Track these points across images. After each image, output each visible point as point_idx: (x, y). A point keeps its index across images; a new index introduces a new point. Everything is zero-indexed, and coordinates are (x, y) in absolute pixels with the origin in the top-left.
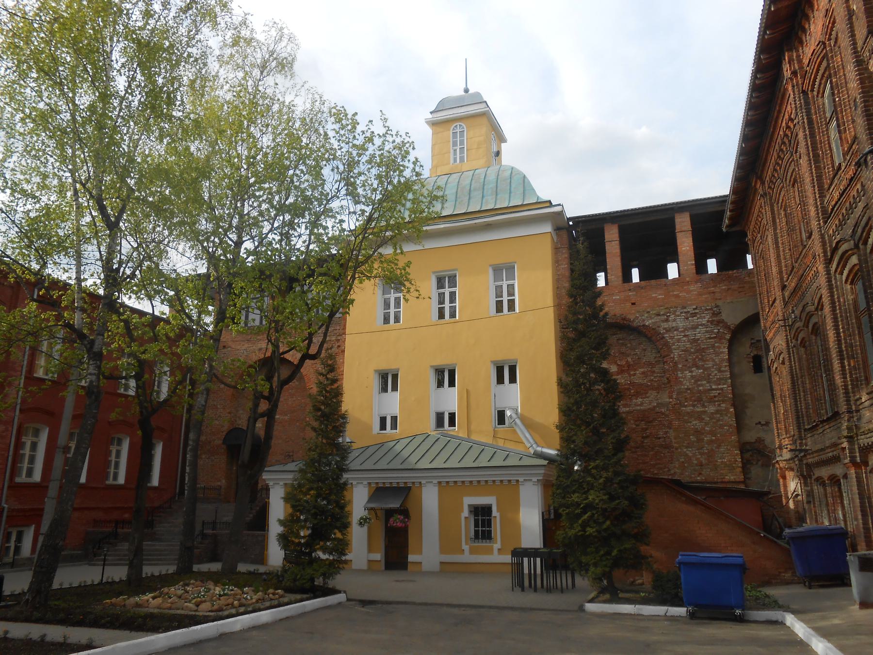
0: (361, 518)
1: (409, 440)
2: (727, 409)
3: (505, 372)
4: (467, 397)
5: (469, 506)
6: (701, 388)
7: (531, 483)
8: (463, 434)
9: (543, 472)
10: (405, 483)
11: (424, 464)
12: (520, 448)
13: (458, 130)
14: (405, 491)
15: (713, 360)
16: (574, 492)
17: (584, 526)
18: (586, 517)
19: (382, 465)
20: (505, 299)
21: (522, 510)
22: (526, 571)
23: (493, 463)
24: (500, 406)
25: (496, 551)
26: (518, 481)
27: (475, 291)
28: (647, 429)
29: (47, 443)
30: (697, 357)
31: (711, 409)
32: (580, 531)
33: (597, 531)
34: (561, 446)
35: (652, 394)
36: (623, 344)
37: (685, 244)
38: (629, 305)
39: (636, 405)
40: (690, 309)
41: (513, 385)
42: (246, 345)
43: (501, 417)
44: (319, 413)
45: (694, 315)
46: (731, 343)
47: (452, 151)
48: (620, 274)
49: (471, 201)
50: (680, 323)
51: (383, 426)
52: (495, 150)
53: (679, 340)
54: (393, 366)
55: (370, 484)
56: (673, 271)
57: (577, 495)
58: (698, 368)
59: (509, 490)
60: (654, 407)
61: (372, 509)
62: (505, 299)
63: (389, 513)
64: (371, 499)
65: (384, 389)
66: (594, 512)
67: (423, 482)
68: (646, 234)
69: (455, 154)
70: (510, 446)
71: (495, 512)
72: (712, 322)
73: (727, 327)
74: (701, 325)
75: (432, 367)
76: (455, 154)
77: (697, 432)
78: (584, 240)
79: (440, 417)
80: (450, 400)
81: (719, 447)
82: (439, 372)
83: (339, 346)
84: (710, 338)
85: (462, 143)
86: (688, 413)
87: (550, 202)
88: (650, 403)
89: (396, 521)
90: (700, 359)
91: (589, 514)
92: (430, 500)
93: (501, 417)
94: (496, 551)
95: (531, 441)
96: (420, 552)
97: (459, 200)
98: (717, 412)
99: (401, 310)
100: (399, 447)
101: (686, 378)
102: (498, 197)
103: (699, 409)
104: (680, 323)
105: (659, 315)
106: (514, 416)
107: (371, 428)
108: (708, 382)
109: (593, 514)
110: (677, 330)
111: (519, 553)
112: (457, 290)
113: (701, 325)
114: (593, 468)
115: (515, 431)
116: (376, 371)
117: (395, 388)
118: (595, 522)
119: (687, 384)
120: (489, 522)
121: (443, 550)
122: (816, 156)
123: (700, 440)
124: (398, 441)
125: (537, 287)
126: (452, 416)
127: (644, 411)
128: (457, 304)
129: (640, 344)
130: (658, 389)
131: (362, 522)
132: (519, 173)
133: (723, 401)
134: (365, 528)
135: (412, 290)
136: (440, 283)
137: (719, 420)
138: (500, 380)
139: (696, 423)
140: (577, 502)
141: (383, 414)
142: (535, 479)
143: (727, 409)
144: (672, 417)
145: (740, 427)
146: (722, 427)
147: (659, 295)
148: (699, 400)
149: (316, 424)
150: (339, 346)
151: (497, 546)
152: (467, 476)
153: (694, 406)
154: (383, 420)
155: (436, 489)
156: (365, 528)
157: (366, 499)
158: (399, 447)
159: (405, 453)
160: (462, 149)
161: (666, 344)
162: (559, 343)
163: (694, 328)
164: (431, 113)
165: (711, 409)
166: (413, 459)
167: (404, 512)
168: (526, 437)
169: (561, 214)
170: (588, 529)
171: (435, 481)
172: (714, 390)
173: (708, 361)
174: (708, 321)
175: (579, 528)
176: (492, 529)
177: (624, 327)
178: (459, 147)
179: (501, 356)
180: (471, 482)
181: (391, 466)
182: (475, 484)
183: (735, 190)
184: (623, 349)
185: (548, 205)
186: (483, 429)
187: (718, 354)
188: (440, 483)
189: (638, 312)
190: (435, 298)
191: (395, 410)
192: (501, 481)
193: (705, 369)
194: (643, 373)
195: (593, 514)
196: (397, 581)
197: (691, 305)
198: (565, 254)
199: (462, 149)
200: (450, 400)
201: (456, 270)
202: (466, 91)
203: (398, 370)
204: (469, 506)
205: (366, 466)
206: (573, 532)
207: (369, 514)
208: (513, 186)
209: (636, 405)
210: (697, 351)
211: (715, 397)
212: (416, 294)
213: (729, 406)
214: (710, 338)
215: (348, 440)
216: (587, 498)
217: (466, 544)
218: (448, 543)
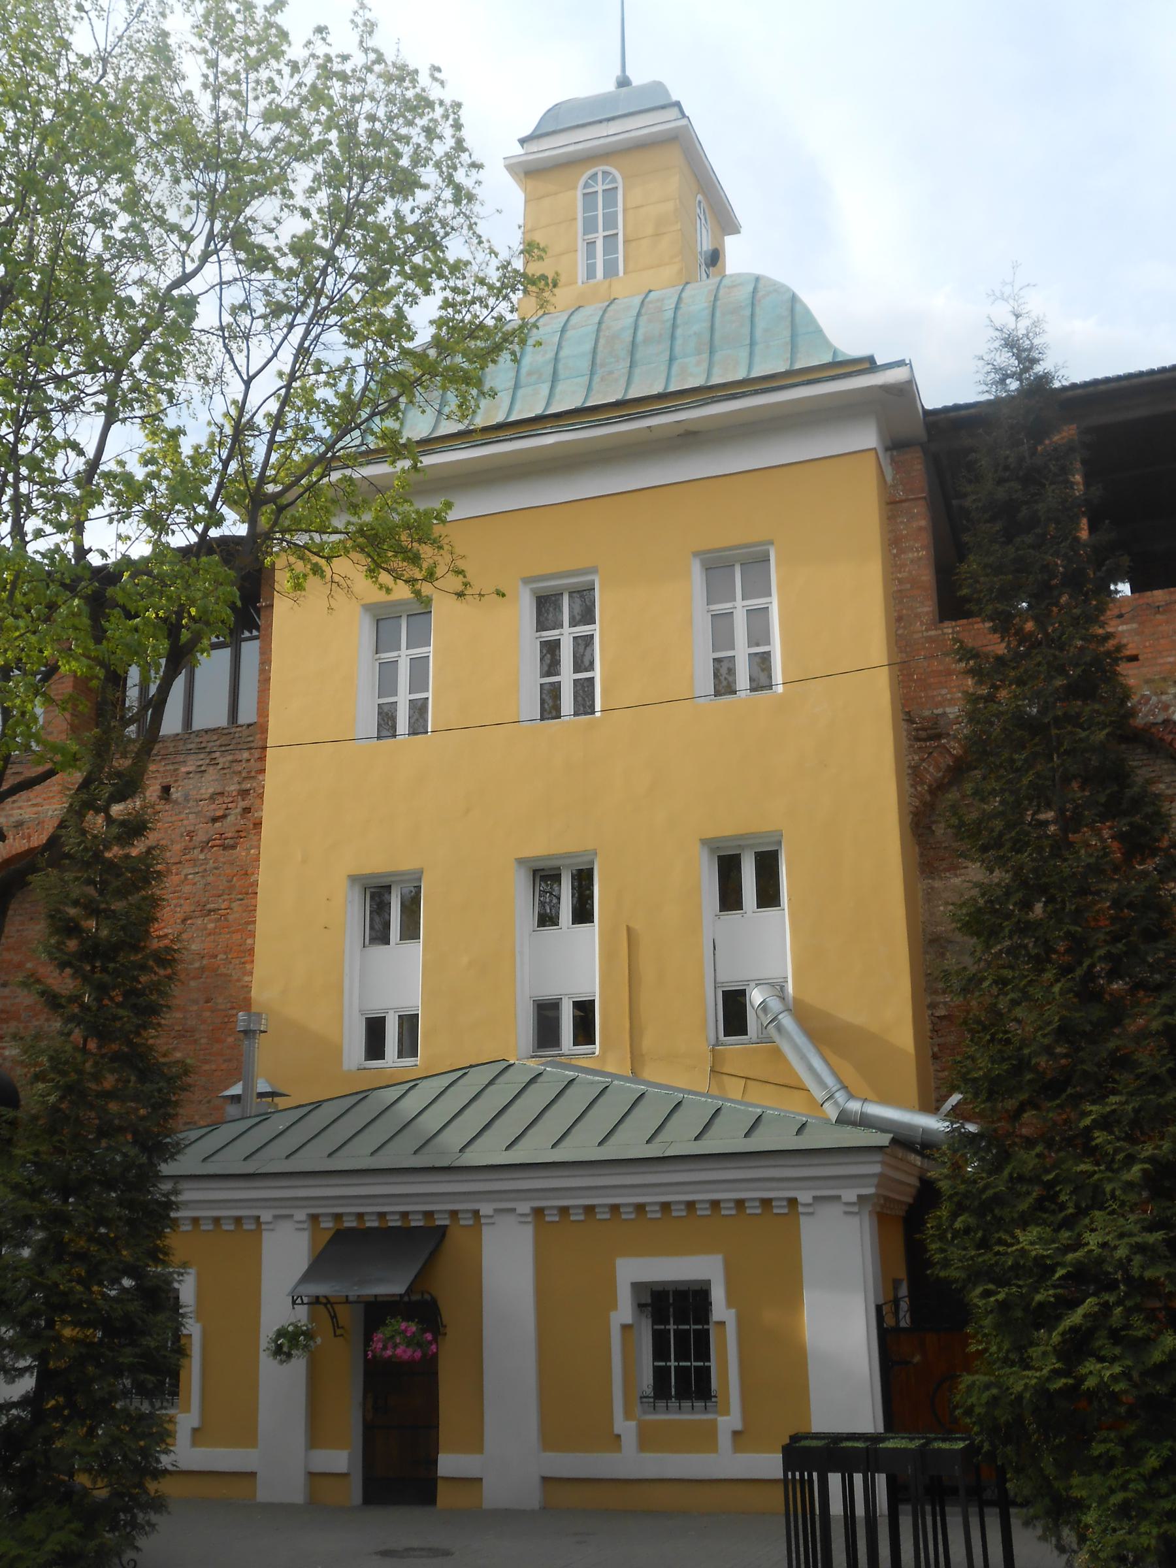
0: (281, 1333)
1: (446, 1080)
3: (745, 874)
4: (628, 950)
5: (637, 1287)
7: (836, 1210)
8: (617, 1064)
9: (877, 1169)
10: (429, 1215)
11: (489, 1152)
12: (795, 1107)
13: (600, 188)
14: (426, 1243)
16: (1024, 1222)
17: (1077, 1347)
18: (1076, 1317)
19: (358, 1156)
21: (811, 1297)
22: (836, 1507)
23: (708, 1146)
24: (731, 978)
25: (724, 1440)
26: (793, 1202)
27: (651, 628)
32: (1056, 1373)
33: (1126, 1375)
41: (770, 913)
43: (734, 1008)
44: (72, 945)
47: (581, 247)
49: (637, 371)
51: (375, 1049)
52: (707, 246)
54: (405, 863)
55: (314, 1218)
57: (1034, 1232)
59: (764, 1229)
61: (316, 1301)
63: (377, 1313)
64: (318, 1267)
65: (380, 935)
66: (1111, 1298)
67: (486, 1209)
69: (591, 254)
70: (764, 1100)
71: (720, 1309)
75: (521, 861)
76: (591, 254)
79: (546, 1016)
80: (577, 962)
82: (544, 877)
83: (247, 810)
85: (610, 221)
87: (871, 360)
89: (398, 1341)
91: (1090, 1304)
92: (507, 1268)
93: (734, 1008)
94: (724, 1440)
95: (830, 1081)
96: (475, 1444)
97: (600, 372)
99: (430, 695)
100: (411, 1105)
102: (718, 357)
106: (775, 1005)
107: (337, 1052)
109: (1106, 1308)
111: (811, 1456)
112: (596, 630)
114: (1096, 1125)
115: (777, 1053)
116: (353, 879)
117: (411, 931)
118: (1115, 1336)
120: (703, 1339)
121: (553, 1436)
124: (414, 1084)
125: (834, 621)
126: (585, 1010)
128: (597, 674)
131: (288, 1343)
132: (778, 289)
134: (298, 1365)
135: (440, 571)
136: (546, 607)
138: (730, 899)
140: (1038, 1260)
141: (375, 1011)
142: (850, 1195)
149: (64, 983)
150: (247, 810)
151: (729, 1421)
152: (627, 1190)
154: (375, 1028)
155: (528, 1232)
156: (298, 1365)
157: (300, 1262)
158: (411, 1105)
159: (431, 1122)
160: (610, 240)
162: (907, 783)
164: (522, 141)
166: (454, 1138)
167: (423, 1310)
168: (811, 1068)
169: (906, 392)
170: (1091, 1365)
171: (524, 1207)
175: (1053, 1363)
176: (713, 1364)
178: (601, 233)
179: (735, 821)
180: (640, 1208)
181: (383, 1161)
182: (654, 1214)
185: (867, 365)
186: (678, 1055)
188: (538, 1212)
189: (1148, 682)
191: (413, 998)
192: (740, 1204)
195: (1106, 1308)
196: (386, 1553)
198: (919, 520)
199: (610, 240)
200: (577, 962)
201: (594, 570)
202: (624, 82)
203: (418, 876)
204: (637, 1287)
205: (308, 1160)
206: (1032, 1377)
207: (312, 1317)
208: (761, 325)
212: (456, 583)
215: (262, 1086)
216: (1078, 1244)
217: (628, 1415)
218: (568, 1412)
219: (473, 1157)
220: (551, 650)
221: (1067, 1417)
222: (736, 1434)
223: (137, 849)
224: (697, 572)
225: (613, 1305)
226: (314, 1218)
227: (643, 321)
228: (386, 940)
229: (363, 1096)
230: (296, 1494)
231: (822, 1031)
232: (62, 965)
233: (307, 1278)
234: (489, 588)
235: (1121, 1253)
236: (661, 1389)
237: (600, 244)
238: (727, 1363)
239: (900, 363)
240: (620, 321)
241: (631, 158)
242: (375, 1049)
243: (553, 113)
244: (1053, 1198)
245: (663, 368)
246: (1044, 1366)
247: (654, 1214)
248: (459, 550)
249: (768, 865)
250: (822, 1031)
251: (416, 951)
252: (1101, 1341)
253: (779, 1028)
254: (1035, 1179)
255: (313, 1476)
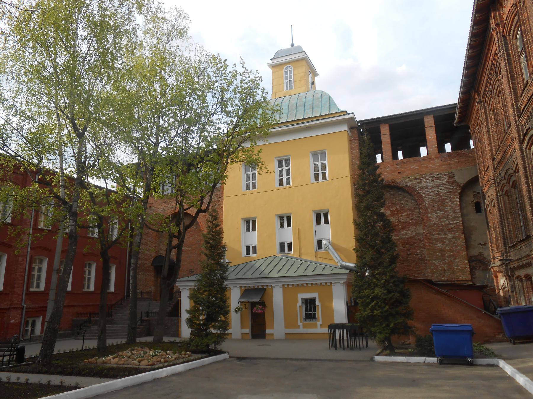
0: (236, 308)
2: (460, 236)
3: (321, 217)
4: (298, 233)
5: (302, 299)
6: (443, 223)
7: (339, 284)
8: (297, 256)
9: (346, 277)
10: (262, 286)
11: (274, 274)
12: (332, 263)
13: (288, 70)
14: (262, 291)
15: (450, 206)
16: (366, 289)
17: (372, 309)
18: (373, 304)
19: (248, 275)
21: (334, 301)
23: (315, 273)
24: (319, 238)
25: (319, 326)
26: (331, 283)
27: (302, 168)
28: (409, 250)
30: (440, 204)
31: (450, 236)
32: (370, 312)
35: (413, 228)
39: (403, 235)
40: (435, 175)
42: (164, 206)
44: (209, 245)
45: (437, 178)
47: (285, 83)
49: (297, 113)
51: (248, 252)
52: (311, 81)
53: (428, 194)
54: (253, 216)
55: (241, 287)
57: (367, 291)
58: (441, 211)
59: (326, 289)
60: (414, 236)
61: (242, 302)
63: (253, 304)
65: (248, 230)
67: (273, 285)
69: (287, 84)
70: (325, 262)
71: (318, 303)
72: (449, 182)
73: (458, 185)
74: (442, 184)
75: (276, 215)
76: (287, 84)
77: (442, 251)
79: (282, 245)
80: (288, 235)
81: (455, 259)
83: (219, 204)
84: (448, 192)
85: (291, 77)
86: (435, 239)
88: (412, 233)
89: (258, 309)
90: (442, 206)
91: (375, 302)
92: (278, 296)
93: (320, 244)
95: (339, 258)
96: (272, 327)
97: (290, 113)
99: (257, 181)
100: (258, 265)
101: (434, 217)
103: (443, 236)
105: (415, 179)
106: (328, 244)
107: (241, 253)
108: (447, 220)
110: (427, 188)
111: (333, 327)
112: (290, 167)
113: (442, 184)
115: (328, 253)
116: (242, 219)
117: (254, 229)
118: (379, 307)
119: (434, 221)
120: (315, 308)
121: (287, 326)
123: (443, 255)
124: (257, 261)
125: (340, 164)
126: (290, 245)
127: (408, 238)
128: (291, 176)
129: (404, 197)
131: (237, 310)
132: (327, 94)
133: (457, 231)
134: (239, 314)
135: (263, 168)
136: (280, 163)
137: (454, 243)
138: (319, 222)
139: (440, 245)
142: (342, 282)
143: (460, 236)
146: (456, 247)
148: (442, 230)
149: (207, 252)
150: (219, 204)
151: (319, 323)
152: (300, 281)
153: (438, 234)
154: (248, 248)
155: (281, 289)
156: (239, 314)
158: (258, 265)
159: (262, 268)
160: (291, 81)
161: (421, 197)
163: (438, 186)
164: (271, 60)
165: (450, 236)
166: (267, 271)
167: (262, 304)
169: (353, 119)
171: (281, 285)
172: (451, 224)
173: (447, 206)
174: (446, 182)
176: (316, 313)
179: (319, 207)
180: (302, 284)
181: (253, 276)
182: (305, 285)
185: (345, 113)
186: (309, 252)
191: (256, 243)
193: (445, 212)
194: (407, 215)
195: (378, 302)
197: (436, 172)
198: (356, 143)
199: (291, 81)
200: (288, 235)
201: (290, 155)
202: (292, 45)
203: (256, 218)
204: (302, 299)
205: (240, 276)
207: (241, 305)
208: (323, 102)
209: (403, 235)
210: (440, 201)
211: (452, 228)
213: (461, 234)
214: (448, 192)
215: (227, 261)
216: (374, 292)
217: (301, 322)
218: (290, 322)
219: (272, 275)
220: (281, 171)
221: (372, 319)
222: (321, 325)
223: (218, 228)
224: (311, 156)
225: (298, 302)
226: (241, 287)
227: (298, 101)
228: (249, 231)
229: (248, 263)
230: (239, 337)
231: (337, 248)
232: (207, 249)
233: (240, 298)
234: (272, 171)
235: (380, 294)
236: (307, 317)
237: (288, 82)
238: (319, 312)
239: (352, 113)
240: (294, 101)
241: (294, 64)
242: (248, 252)
243: (277, 53)
244: (370, 285)
245: (303, 112)
246: (368, 312)
247: (305, 285)
248: (266, 164)
249: (326, 215)
250: (337, 248)
251: (256, 233)
252: (377, 308)
253: (329, 248)
254: (367, 282)
255: (242, 334)
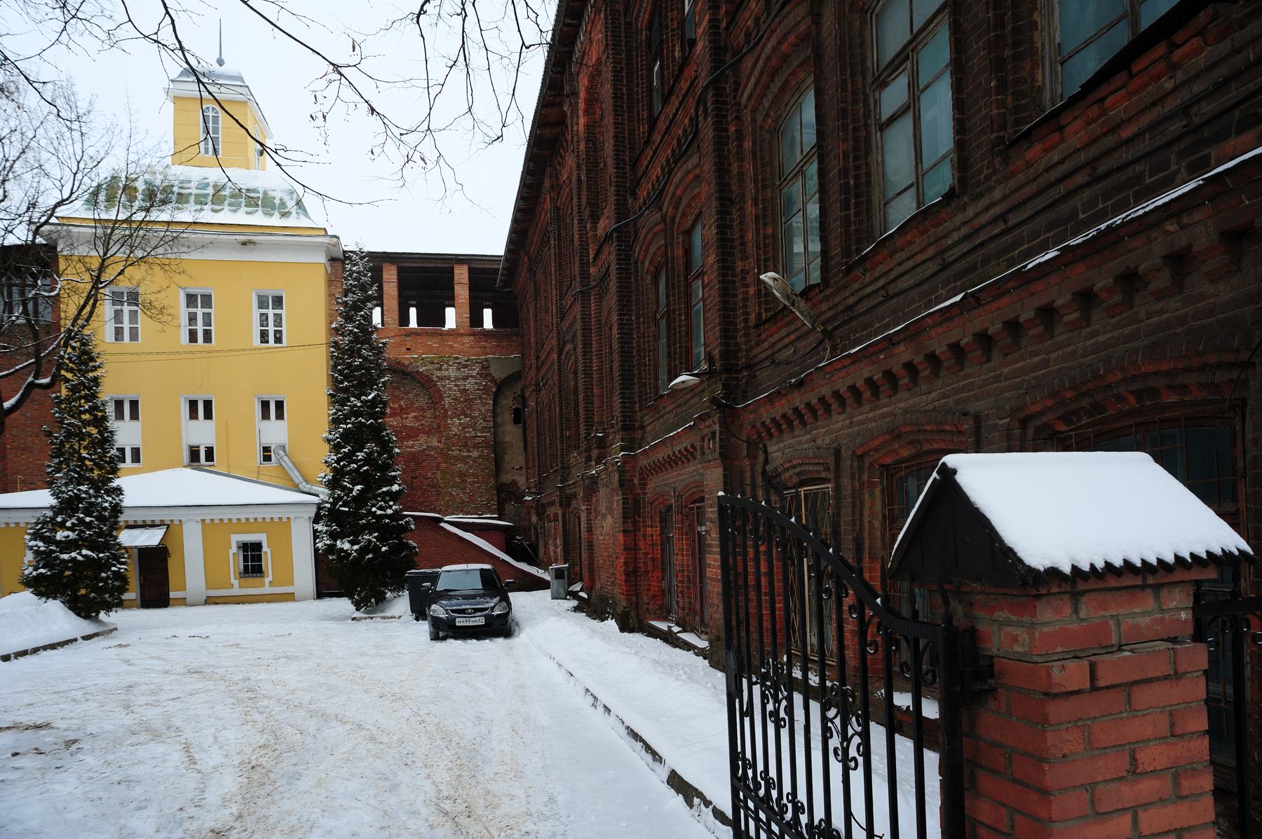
20: (271, 329)
29: (14, 490)
31: (475, 454)
34: (1218, 815)
35: (423, 438)
36: (396, 388)
37: (462, 292)
38: (404, 349)
43: (267, 454)
45: (465, 366)
46: (496, 397)
48: (397, 317)
50: (452, 373)
53: (450, 389)
56: (450, 314)
62: (271, 329)
67: (292, 517)
68: (425, 279)
71: (265, 548)
72: (481, 375)
73: (493, 380)
77: (462, 475)
78: (361, 279)
88: (421, 445)
98: (480, 457)
101: (455, 425)
104: (452, 373)
119: (455, 430)
122: (560, 264)
123: (464, 481)
125: (310, 318)
130: (428, 433)
144: (439, 460)
145: (498, 472)
147: (434, 343)
148: (465, 445)
163: (465, 378)
177: (401, 372)
183: (508, 250)
184: (397, 393)
187: (484, 404)
190: (184, 320)
193: (472, 418)
